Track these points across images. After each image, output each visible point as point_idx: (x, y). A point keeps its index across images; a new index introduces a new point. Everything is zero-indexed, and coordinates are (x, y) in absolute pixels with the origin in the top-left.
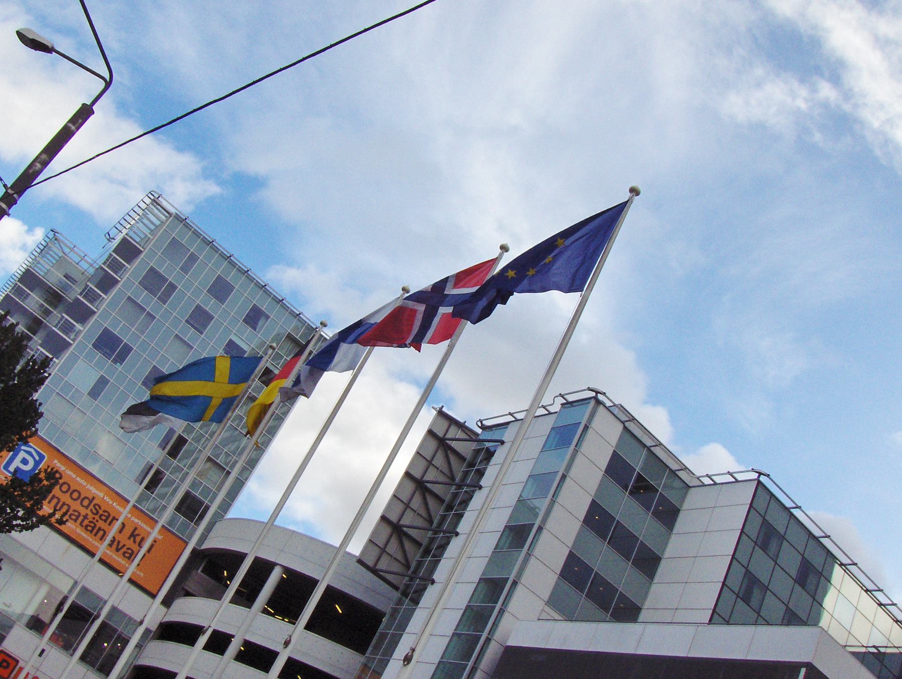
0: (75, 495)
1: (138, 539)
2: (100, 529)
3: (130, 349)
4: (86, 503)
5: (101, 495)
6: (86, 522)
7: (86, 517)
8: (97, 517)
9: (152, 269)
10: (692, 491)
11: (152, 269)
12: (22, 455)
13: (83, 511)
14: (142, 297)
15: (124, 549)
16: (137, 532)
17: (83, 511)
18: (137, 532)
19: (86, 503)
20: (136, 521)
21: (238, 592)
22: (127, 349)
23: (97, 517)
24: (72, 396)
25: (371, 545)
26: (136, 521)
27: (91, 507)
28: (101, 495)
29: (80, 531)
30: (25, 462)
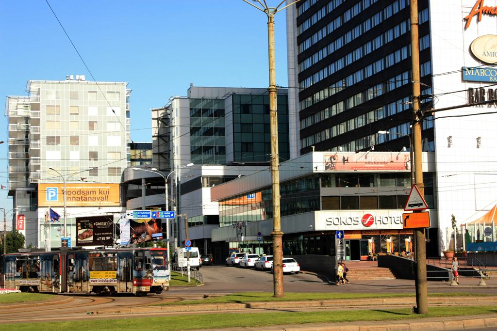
0: (74, 193)
1: (102, 192)
2: (89, 198)
3: (59, 137)
4: (79, 193)
5: (82, 187)
6: (83, 198)
7: (82, 197)
8: (85, 195)
9: (78, 99)
10: (225, 100)
11: (78, 99)
12: (50, 192)
13: (80, 196)
14: (51, 117)
15: (100, 199)
16: (101, 191)
17: (80, 196)
18: (101, 191)
19: (79, 193)
20: (98, 187)
21: (281, 212)
22: (58, 137)
23: (85, 195)
24: (76, 165)
25: (154, 155)
26: (98, 187)
27: (81, 193)
28: (82, 187)
29: (77, 202)
30: (52, 194)
